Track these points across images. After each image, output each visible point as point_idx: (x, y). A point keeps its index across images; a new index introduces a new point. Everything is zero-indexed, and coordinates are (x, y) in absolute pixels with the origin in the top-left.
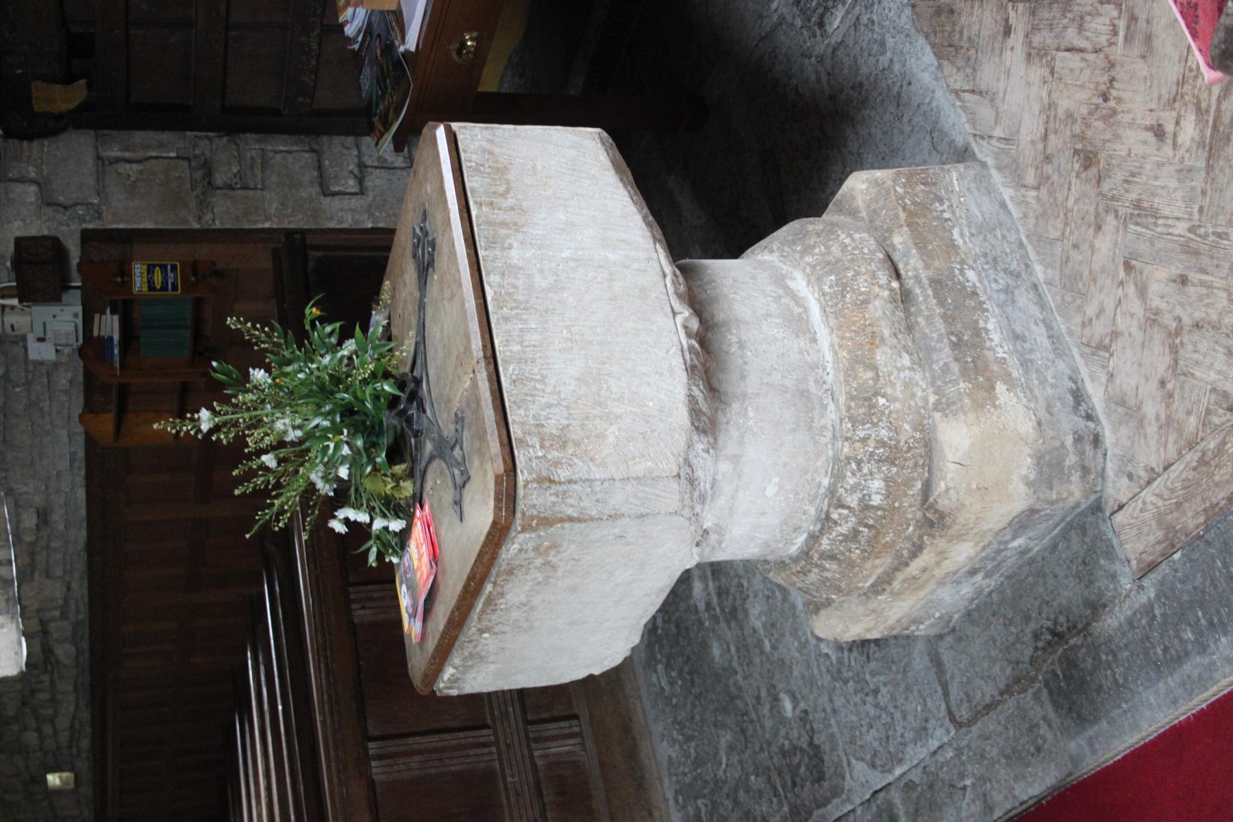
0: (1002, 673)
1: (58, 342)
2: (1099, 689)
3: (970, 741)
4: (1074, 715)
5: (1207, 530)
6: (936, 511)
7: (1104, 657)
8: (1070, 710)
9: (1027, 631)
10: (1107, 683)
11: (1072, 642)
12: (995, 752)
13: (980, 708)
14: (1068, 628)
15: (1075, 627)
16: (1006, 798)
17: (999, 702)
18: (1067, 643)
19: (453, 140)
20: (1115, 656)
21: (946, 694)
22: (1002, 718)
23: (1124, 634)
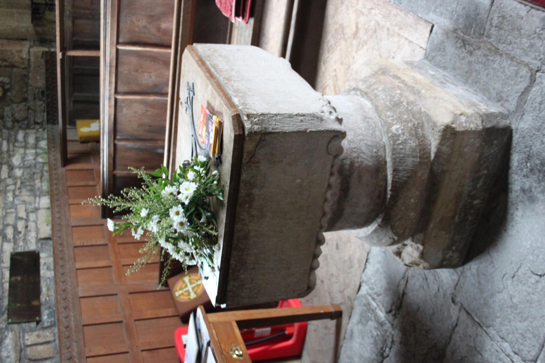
0: (498, 62)
1: (168, 292)
2: (464, 8)
3: (533, 59)
4: (478, 11)
5: (410, 11)
6: (379, 71)
7: (456, 16)
8: (478, 14)
9: (473, 59)
10: (460, 7)
11: (462, 34)
12: (524, 40)
13: (515, 63)
14: (459, 39)
15: (457, 37)
16: (532, 16)
17: (507, 54)
18: (463, 36)
19: (201, 62)
20: (452, 12)
21: (527, 90)
22: (510, 47)
23: (445, 15)
